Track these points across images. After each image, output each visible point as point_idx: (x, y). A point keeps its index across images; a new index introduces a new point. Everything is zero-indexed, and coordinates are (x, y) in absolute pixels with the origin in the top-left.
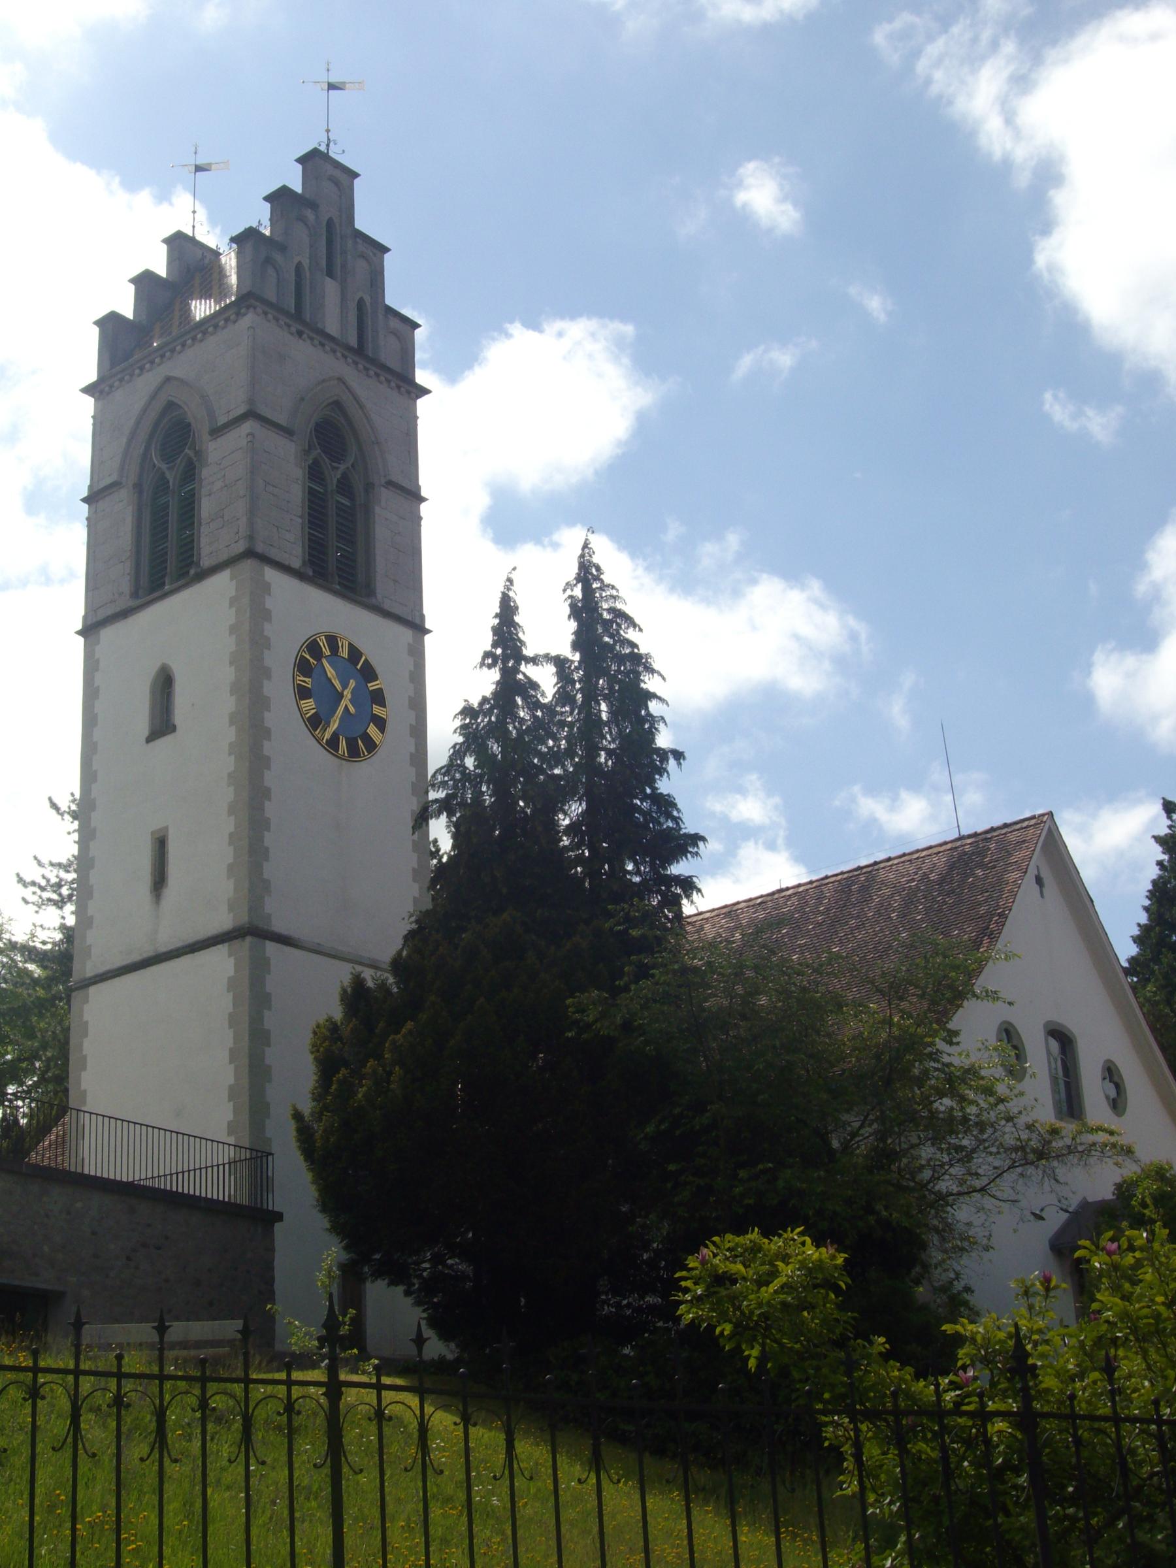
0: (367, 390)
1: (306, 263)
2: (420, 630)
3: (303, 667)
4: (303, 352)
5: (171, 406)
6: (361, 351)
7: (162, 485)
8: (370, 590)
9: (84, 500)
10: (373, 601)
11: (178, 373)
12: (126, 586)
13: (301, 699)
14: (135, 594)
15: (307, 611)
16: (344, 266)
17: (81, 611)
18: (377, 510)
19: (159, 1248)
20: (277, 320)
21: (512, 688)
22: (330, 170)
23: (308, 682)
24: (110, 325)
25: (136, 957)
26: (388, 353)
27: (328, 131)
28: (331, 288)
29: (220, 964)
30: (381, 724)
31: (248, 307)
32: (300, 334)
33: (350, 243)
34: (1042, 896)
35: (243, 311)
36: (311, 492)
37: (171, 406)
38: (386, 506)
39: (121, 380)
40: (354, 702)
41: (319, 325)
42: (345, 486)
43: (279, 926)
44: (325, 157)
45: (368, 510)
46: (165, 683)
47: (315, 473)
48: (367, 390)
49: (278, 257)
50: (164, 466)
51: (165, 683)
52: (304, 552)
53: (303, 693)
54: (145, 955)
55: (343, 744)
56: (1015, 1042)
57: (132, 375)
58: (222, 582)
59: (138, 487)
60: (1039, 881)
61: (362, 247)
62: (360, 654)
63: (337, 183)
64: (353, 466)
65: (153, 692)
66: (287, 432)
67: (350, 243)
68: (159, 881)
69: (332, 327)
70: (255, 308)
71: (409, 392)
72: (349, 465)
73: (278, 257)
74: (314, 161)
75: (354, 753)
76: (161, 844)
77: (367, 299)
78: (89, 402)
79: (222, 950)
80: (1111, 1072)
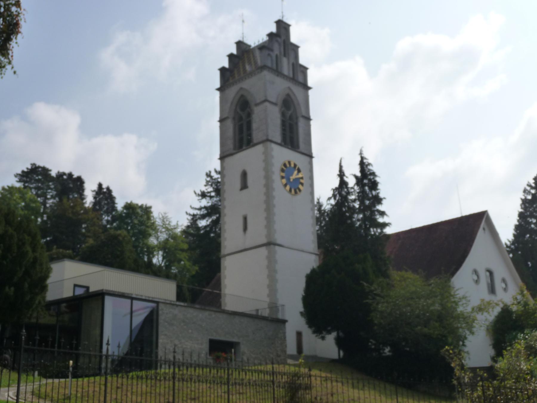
0: (297, 91)
1: (278, 54)
2: (311, 156)
4: (279, 80)
5: (242, 96)
6: (293, 80)
7: (241, 119)
10: (299, 150)
15: (282, 155)
21: (343, 183)
24: (223, 70)
26: (300, 79)
28: (285, 60)
29: (263, 251)
30: (302, 184)
37: (242, 96)
38: (301, 123)
40: (298, 181)
42: (291, 118)
43: (279, 242)
45: (297, 124)
47: (283, 114)
48: (297, 91)
51: (244, 175)
55: (293, 191)
58: (259, 148)
59: (234, 119)
60: (484, 229)
66: (275, 104)
68: (245, 229)
75: (296, 193)
76: (245, 219)
80: (504, 280)
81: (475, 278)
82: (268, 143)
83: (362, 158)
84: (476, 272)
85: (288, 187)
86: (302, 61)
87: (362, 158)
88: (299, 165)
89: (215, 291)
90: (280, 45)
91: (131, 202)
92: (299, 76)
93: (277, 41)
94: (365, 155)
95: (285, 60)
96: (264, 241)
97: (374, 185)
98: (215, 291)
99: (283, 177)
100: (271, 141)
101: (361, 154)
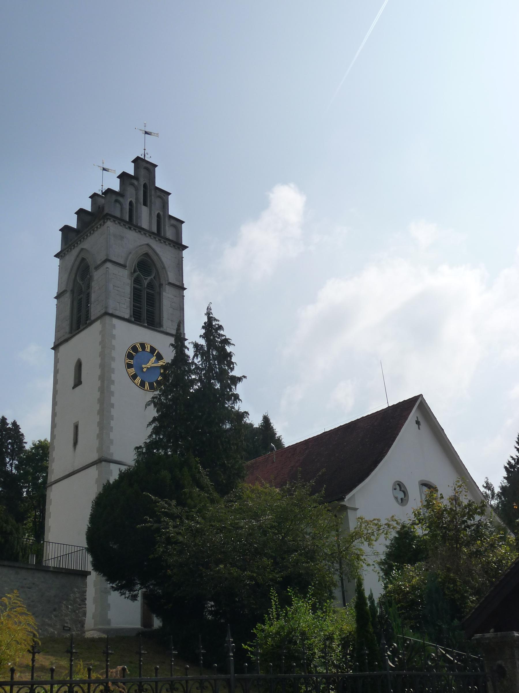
1: (134, 201)
3: (130, 356)
6: (158, 234)
8: (160, 325)
9: (55, 298)
10: (162, 329)
11: (85, 247)
12: (67, 329)
13: (128, 368)
14: (71, 332)
16: (151, 201)
17: (53, 340)
18: (164, 293)
19: (30, 588)
20: (120, 223)
22: (145, 165)
23: (132, 362)
24: (66, 230)
25: (67, 473)
26: (169, 233)
27: (145, 150)
28: (144, 211)
31: (107, 219)
32: (130, 228)
33: (153, 192)
34: (419, 429)
35: (106, 221)
36: (135, 288)
39: (68, 251)
41: (139, 225)
43: (116, 458)
44: (144, 160)
45: (160, 294)
46: (79, 365)
47: (137, 281)
49: (121, 199)
50: (81, 283)
51: (79, 365)
52: (131, 312)
53: (129, 366)
54: (71, 472)
56: (403, 489)
57: (71, 249)
58: (97, 326)
59: (72, 291)
60: (418, 423)
61: (158, 193)
62: (156, 350)
63: (147, 169)
64: (154, 278)
65: (75, 369)
66: (124, 266)
67: (153, 192)
68: (75, 443)
69: (145, 225)
70: (110, 219)
71: (179, 248)
72: (152, 277)
73: (121, 199)
74: (137, 161)
76: (76, 427)
77: (161, 213)
78: (57, 261)
79: (95, 467)
81: (401, 495)
82: (107, 318)
83: (210, 319)
84: (400, 486)
85: (138, 380)
86: (174, 211)
87: (210, 319)
88: (159, 349)
89: (448, 655)
90: (137, 189)
91: (115, 480)
92: (169, 233)
93: (133, 184)
94: (215, 314)
95: (144, 211)
96: (95, 457)
97: (225, 358)
98: (448, 655)
99: (129, 366)
100: (112, 315)
101: (208, 314)
